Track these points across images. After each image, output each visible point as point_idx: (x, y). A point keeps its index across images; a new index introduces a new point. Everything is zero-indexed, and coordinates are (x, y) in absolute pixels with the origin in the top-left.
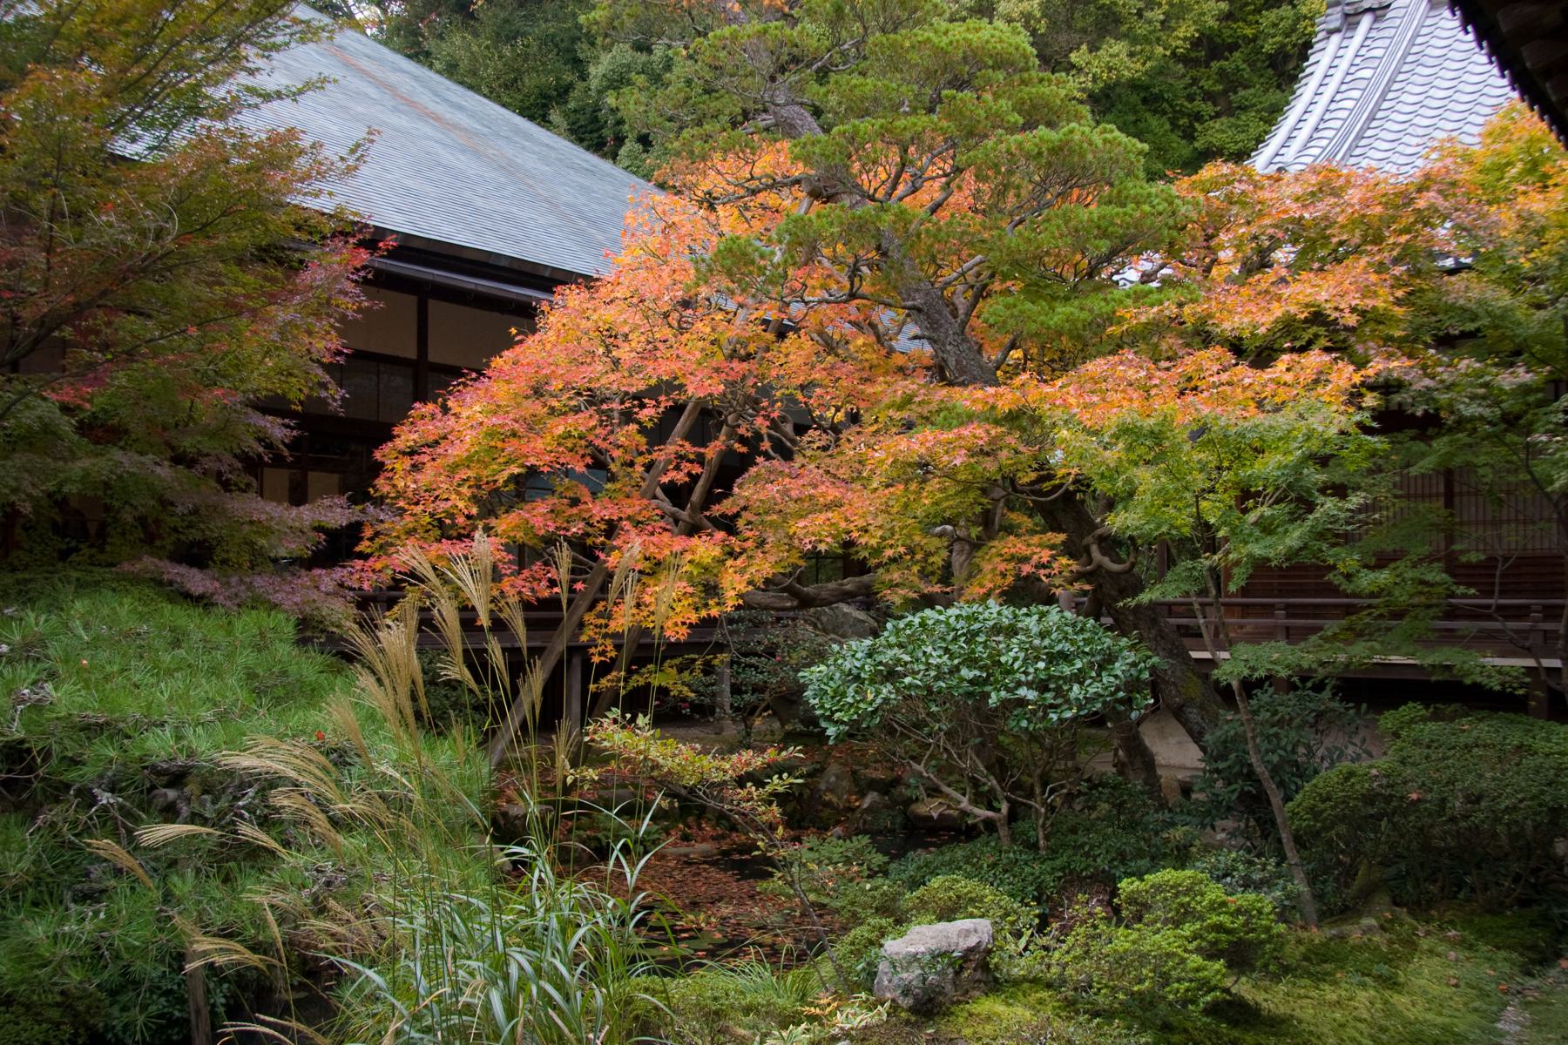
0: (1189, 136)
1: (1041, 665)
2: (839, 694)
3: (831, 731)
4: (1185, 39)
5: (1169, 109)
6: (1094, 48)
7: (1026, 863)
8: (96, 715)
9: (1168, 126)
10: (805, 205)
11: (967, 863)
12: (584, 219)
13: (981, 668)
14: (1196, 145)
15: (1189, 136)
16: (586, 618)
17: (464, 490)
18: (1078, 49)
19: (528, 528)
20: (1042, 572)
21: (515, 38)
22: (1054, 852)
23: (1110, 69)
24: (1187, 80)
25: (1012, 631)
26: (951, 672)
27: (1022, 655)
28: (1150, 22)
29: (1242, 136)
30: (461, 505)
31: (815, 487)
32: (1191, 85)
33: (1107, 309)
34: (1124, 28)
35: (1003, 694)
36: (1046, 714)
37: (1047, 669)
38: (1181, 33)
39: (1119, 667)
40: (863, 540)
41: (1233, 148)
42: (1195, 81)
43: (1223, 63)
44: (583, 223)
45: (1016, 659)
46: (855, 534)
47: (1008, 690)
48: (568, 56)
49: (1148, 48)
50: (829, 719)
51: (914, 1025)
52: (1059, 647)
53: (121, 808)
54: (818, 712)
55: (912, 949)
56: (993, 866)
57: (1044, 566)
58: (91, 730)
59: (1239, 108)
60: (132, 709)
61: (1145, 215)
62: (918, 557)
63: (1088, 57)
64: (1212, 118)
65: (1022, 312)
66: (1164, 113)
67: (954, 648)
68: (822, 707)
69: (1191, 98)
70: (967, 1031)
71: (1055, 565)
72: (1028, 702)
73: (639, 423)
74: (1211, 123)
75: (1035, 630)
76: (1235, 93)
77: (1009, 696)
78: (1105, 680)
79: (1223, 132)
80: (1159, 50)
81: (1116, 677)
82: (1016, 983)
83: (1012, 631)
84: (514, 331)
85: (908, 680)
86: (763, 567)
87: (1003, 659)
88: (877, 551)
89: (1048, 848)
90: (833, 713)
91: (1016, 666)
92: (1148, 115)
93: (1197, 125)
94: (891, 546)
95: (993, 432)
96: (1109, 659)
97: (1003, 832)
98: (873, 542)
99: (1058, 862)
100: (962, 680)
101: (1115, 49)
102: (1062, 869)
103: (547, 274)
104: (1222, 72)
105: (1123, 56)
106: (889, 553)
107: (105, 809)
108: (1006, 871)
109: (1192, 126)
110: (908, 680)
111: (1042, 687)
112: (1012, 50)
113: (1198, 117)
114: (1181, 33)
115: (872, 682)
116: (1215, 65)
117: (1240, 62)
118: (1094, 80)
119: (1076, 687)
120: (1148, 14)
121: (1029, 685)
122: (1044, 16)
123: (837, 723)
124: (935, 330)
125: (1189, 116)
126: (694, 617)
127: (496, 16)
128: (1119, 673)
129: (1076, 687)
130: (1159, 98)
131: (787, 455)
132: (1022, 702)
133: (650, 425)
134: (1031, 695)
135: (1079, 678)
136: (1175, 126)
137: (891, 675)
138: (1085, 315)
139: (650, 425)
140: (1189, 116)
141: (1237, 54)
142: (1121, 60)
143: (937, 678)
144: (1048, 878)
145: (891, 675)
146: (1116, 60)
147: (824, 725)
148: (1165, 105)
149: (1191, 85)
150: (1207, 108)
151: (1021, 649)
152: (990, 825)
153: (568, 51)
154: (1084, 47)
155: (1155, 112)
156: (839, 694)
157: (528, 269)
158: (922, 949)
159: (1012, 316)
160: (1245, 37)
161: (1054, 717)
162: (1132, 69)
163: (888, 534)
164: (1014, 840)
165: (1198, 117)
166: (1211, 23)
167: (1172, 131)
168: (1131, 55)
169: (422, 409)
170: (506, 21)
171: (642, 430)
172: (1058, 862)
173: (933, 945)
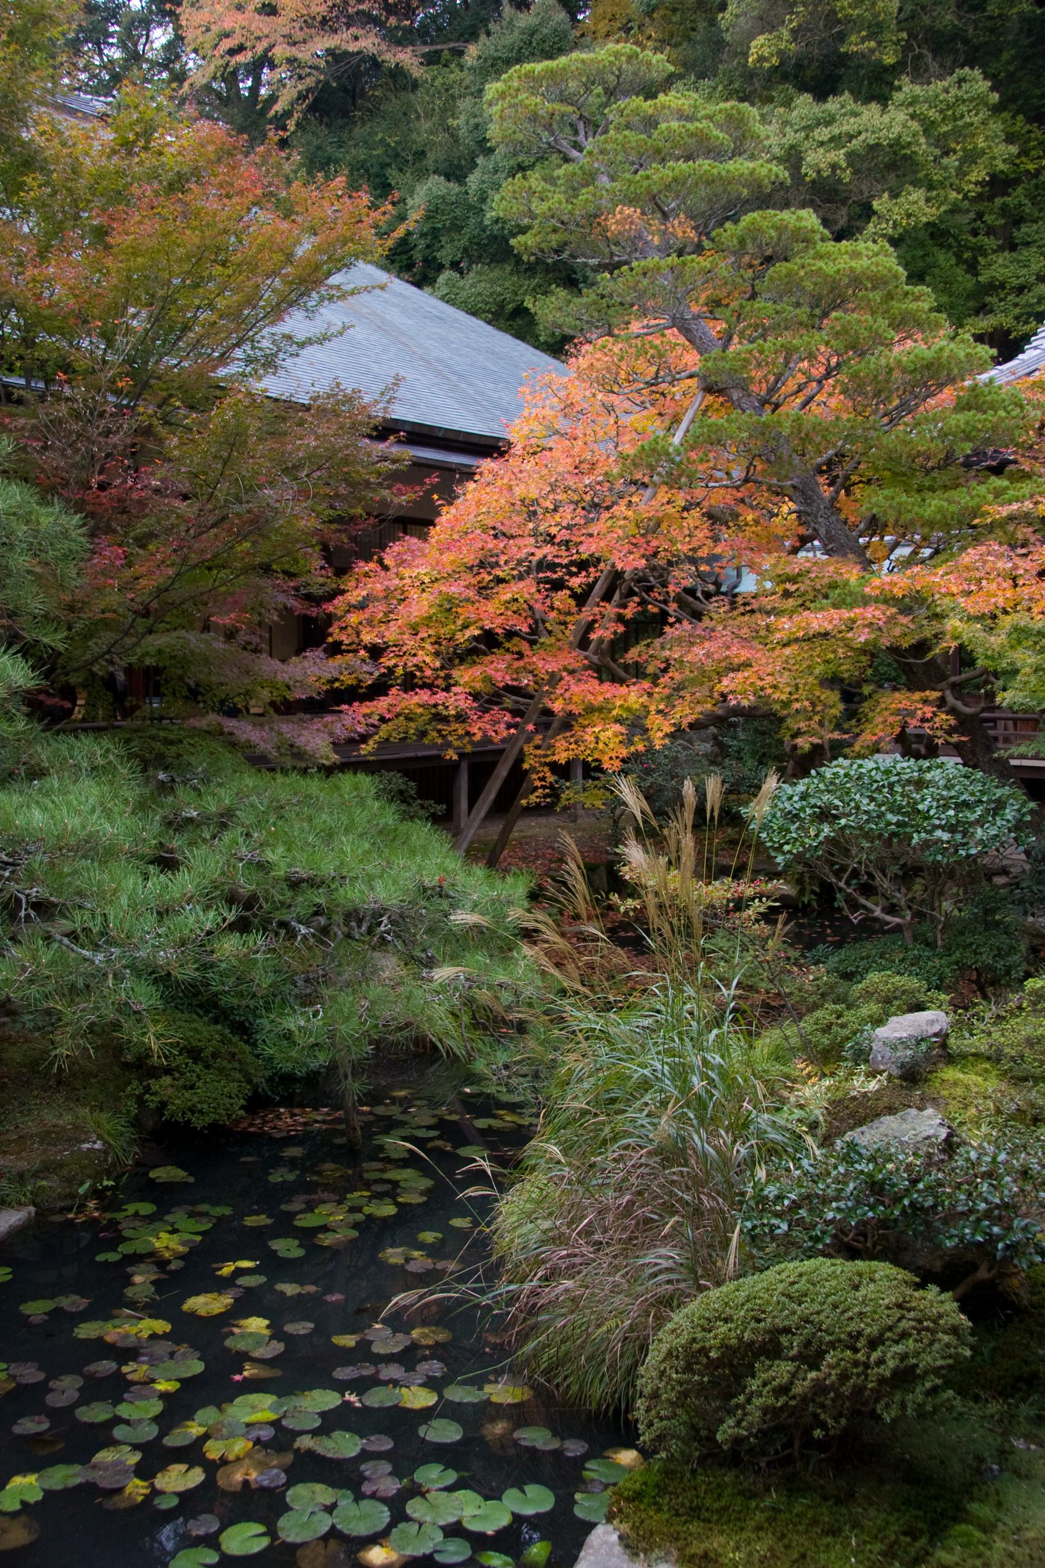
0: (972, 268)
1: (951, 812)
2: (784, 830)
3: (780, 859)
4: (977, 183)
5: (954, 244)
6: (895, 195)
7: (929, 959)
8: (302, 871)
9: (953, 261)
10: (699, 398)
11: (881, 957)
12: (455, 373)
13: (903, 814)
14: (980, 278)
15: (972, 268)
16: (526, 749)
17: (428, 647)
18: (880, 197)
19: (488, 680)
20: (926, 725)
21: (328, 164)
22: (948, 951)
23: (909, 216)
24: (972, 215)
25: (920, 784)
26: (879, 817)
27: (935, 804)
28: (946, 168)
29: (1024, 271)
30: (428, 659)
31: (728, 648)
32: (975, 220)
33: (972, 503)
34: (921, 175)
35: (923, 835)
36: (957, 851)
37: (956, 815)
38: (973, 177)
39: (1009, 813)
40: (776, 696)
41: (1015, 282)
42: (980, 216)
43: (1007, 199)
44: (454, 378)
45: (931, 807)
46: (769, 691)
47: (927, 832)
48: (377, 180)
49: (942, 193)
50: (776, 849)
51: (906, 1088)
52: (962, 798)
53: (314, 935)
54: (769, 844)
55: (897, 1035)
56: (902, 960)
57: (928, 721)
58: (295, 884)
59: (1023, 244)
60: (328, 868)
61: (1002, 419)
62: (819, 708)
63: (890, 205)
64: (994, 251)
65: (900, 504)
66: (950, 247)
67: (879, 797)
68: (771, 840)
69: (975, 233)
70: (945, 1093)
71: (937, 719)
72: (943, 842)
73: (571, 589)
74: (994, 257)
75: (942, 783)
76: (1019, 229)
77: (928, 837)
78: (999, 823)
79: (1007, 267)
80: (953, 195)
81: (1008, 821)
82: (964, 1056)
83: (920, 784)
84: (436, 497)
85: (843, 821)
86: (685, 713)
87: (920, 807)
88: (786, 704)
89: (944, 947)
90: (782, 845)
91: (932, 812)
92: (935, 249)
93: (980, 259)
94: (797, 700)
95: (888, 613)
96: (1000, 805)
97: (908, 934)
98: (784, 697)
99: (953, 958)
100: (889, 824)
101: (914, 197)
102: (957, 963)
103: (440, 435)
104: (1004, 208)
105: (922, 203)
106: (797, 705)
107: (304, 936)
108: (912, 965)
109: (975, 258)
110: (843, 821)
111: (952, 829)
112: (885, 272)
113: (981, 250)
114: (973, 177)
115: (812, 822)
116: (999, 201)
117: (1022, 198)
118: (894, 227)
119: (979, 830)
120: (945, 161)
121: (942, 827)
122: (849, 165)
123: (784, 853)
124: (808, 505)
125: (973, 249)
126: (624, 752)
127: (309, 143)
128: (1009, 817)
129: (979, 830)
130: (946, 233)
131: (697, 616)
132: (940, 840)
133: (579, 591)
134: (946, 836)
135: (980, 822)
136: (958, 256)
137: (825, 815)
138: (953, 508)
139: (579, 591)
140: (973, 249)
141: (1020, 190)
142: (919, 208)
143: (867, 821)
144: (947, 970)
145: (825, 815)
146: (915, 207)
147: (773, 854)
148: (951, 240)
149: (975, 220)
150: (991, 242)
151: (933, 799)
152: (898, 929)
153: (377, 176)
154: (886, 195)
155: (941, 246)
156: (784, 830)
157: (425, 431)
158: (905, 1035)
159: (891, 507)
160: (1028, 171)
161: (963, 853)
162: (929, 213)
163: (793, 690)
164: (915, 940)
165: (981, 250)
166: (1002, 166)
167: (957, 265)
168: (928, 200)
169: (363, 567)
170: (319, 148)
171: (574, 595)
172: (953, 958)
173: (911, 1031)
